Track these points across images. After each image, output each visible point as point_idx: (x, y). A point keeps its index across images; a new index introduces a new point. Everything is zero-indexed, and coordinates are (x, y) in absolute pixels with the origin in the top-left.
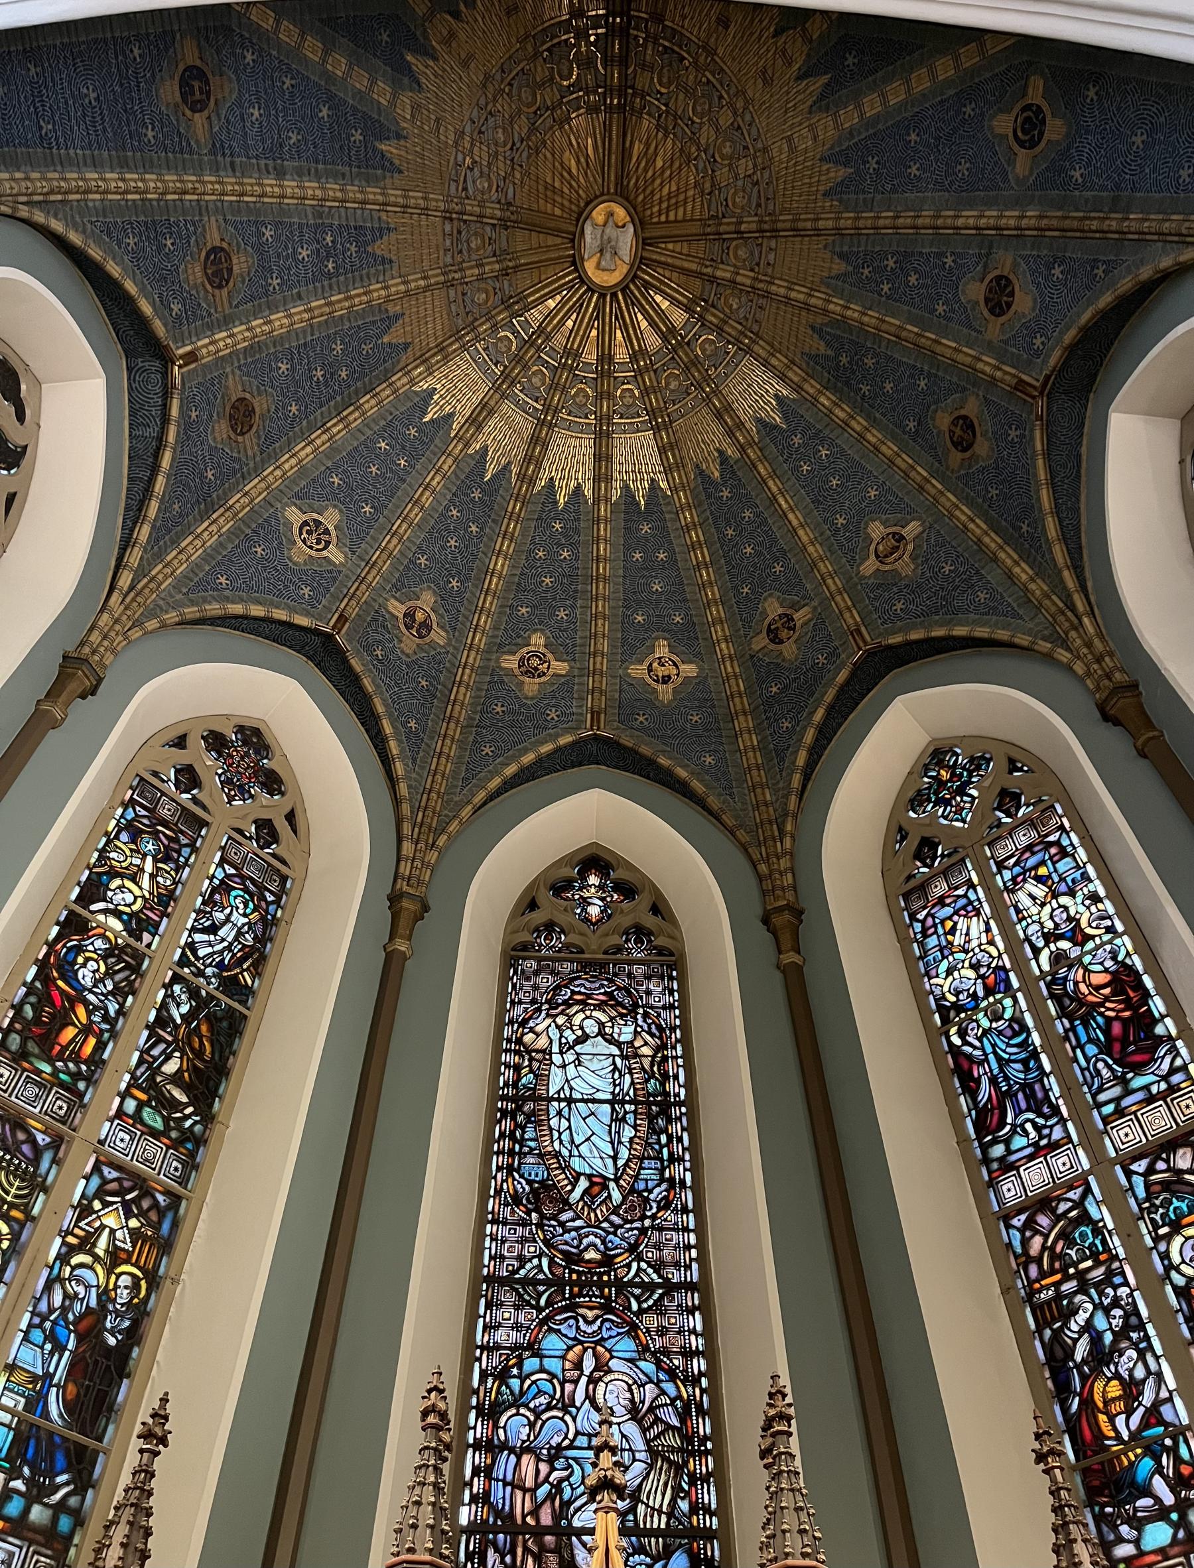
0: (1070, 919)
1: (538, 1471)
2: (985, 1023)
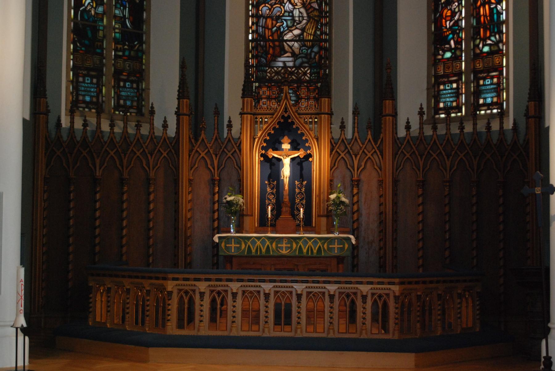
1: (272, 23)
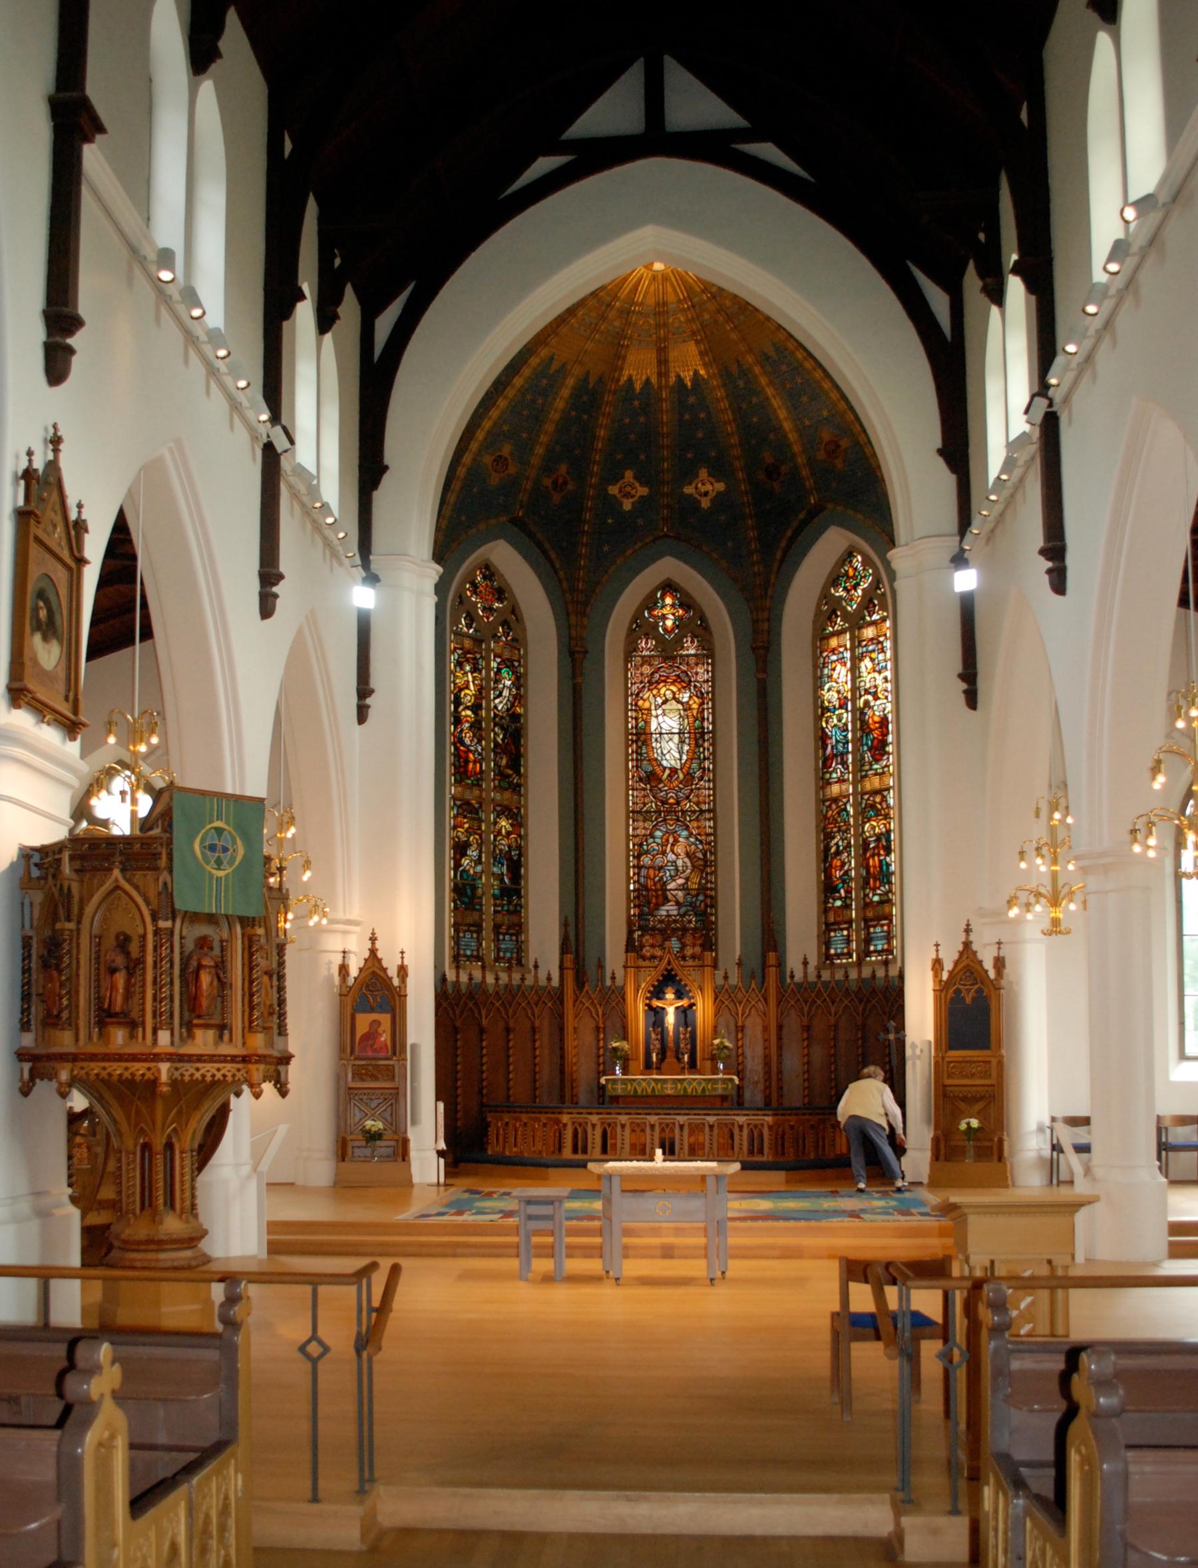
0: (876, 687)
2: (835, 721)
